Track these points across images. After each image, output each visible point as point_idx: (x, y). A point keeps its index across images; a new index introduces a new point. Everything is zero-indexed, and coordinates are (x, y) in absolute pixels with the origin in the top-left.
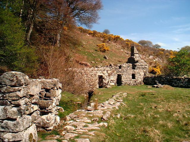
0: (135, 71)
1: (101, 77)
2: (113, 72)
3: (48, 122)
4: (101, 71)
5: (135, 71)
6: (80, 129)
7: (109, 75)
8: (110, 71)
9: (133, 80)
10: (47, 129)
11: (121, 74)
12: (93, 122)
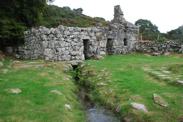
1: (85, 42)
2: (103, 34)
4: (86, 33)
7: (98, 39)
8: (99, 33)
9: (125, 46)
11: (112, 38)
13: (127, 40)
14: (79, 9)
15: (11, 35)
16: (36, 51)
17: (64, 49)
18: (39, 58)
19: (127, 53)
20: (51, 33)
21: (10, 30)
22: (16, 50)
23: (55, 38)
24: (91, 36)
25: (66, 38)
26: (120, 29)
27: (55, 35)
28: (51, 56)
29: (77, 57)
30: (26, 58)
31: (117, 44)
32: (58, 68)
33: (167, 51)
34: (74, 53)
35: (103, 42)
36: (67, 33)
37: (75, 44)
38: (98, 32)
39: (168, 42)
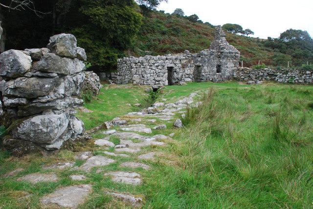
0: (221, 60)
1: (170, 69)
2: (189, 62)
3: (45, 130)
4: (171, 60)
5: (221, 60)
6: (124, 146)
7: (184, 66)
8: (185, 61)
9: (217, 73)
10: (47, 146)
11: (201, 64)
12: (155, 132)
13: (221, 67)
14: (193, 15)
15: (106, 63)
16: (127, 76)
17: (149, 75)
18: (129, 82)
19: (219, 81)
20: (139, 62)
21: (104, 58)
22: (109, 76)
23: (142, 66)
24: (175, 64)
25: (151, 66)
26: (212, 55)
27: (142, 63)
28: (138, 81)
29: (160, 82)
30: (119, 82)
31: (207, 71)
32: (142, 89)
33: (263, 79)
34: (158, 79)
35: (189, 69)
36: (152, 61)
37: (160, 71)
38: (183, 59)
39: (266, 69)
